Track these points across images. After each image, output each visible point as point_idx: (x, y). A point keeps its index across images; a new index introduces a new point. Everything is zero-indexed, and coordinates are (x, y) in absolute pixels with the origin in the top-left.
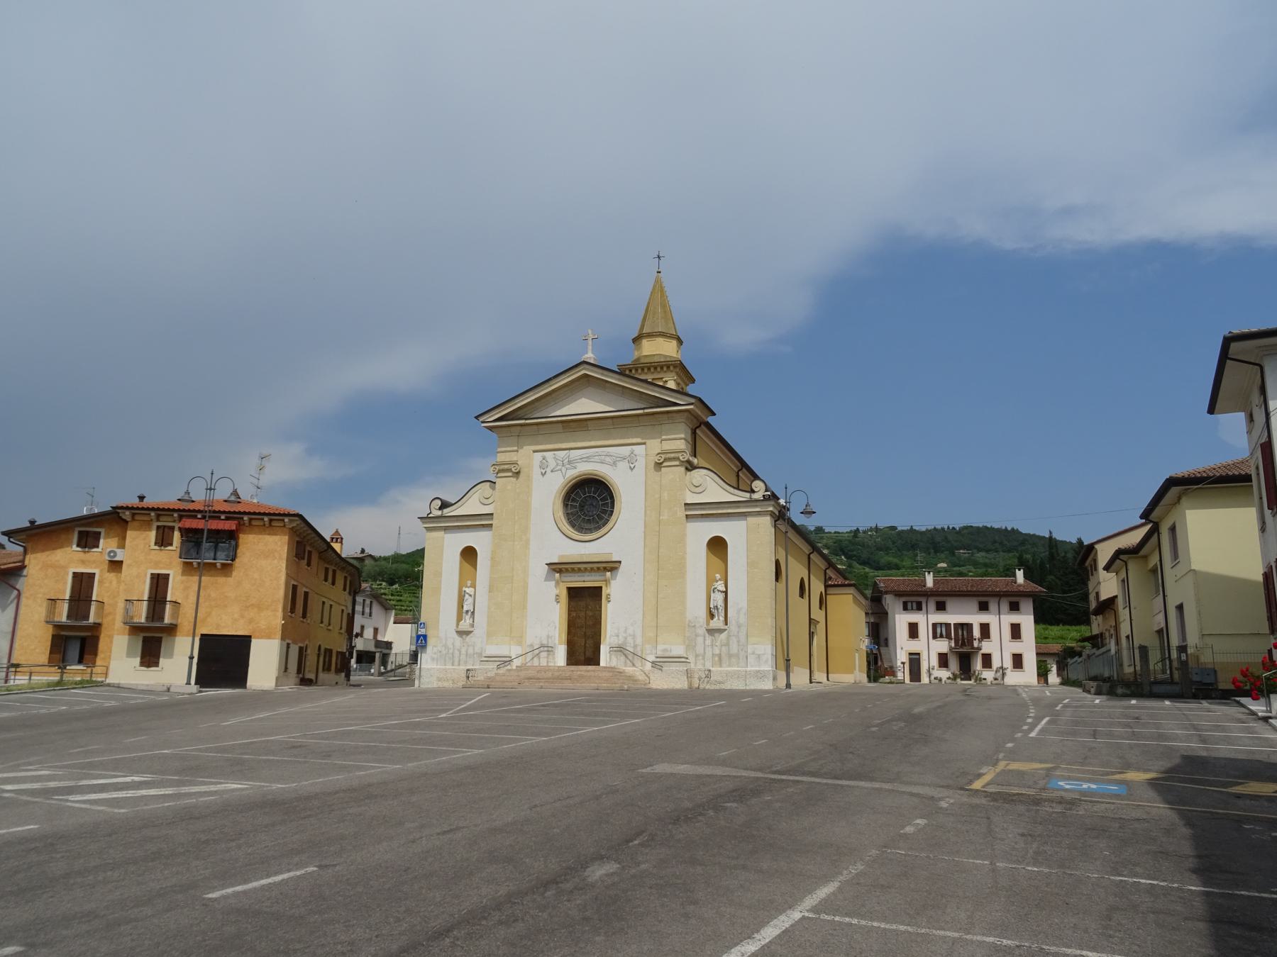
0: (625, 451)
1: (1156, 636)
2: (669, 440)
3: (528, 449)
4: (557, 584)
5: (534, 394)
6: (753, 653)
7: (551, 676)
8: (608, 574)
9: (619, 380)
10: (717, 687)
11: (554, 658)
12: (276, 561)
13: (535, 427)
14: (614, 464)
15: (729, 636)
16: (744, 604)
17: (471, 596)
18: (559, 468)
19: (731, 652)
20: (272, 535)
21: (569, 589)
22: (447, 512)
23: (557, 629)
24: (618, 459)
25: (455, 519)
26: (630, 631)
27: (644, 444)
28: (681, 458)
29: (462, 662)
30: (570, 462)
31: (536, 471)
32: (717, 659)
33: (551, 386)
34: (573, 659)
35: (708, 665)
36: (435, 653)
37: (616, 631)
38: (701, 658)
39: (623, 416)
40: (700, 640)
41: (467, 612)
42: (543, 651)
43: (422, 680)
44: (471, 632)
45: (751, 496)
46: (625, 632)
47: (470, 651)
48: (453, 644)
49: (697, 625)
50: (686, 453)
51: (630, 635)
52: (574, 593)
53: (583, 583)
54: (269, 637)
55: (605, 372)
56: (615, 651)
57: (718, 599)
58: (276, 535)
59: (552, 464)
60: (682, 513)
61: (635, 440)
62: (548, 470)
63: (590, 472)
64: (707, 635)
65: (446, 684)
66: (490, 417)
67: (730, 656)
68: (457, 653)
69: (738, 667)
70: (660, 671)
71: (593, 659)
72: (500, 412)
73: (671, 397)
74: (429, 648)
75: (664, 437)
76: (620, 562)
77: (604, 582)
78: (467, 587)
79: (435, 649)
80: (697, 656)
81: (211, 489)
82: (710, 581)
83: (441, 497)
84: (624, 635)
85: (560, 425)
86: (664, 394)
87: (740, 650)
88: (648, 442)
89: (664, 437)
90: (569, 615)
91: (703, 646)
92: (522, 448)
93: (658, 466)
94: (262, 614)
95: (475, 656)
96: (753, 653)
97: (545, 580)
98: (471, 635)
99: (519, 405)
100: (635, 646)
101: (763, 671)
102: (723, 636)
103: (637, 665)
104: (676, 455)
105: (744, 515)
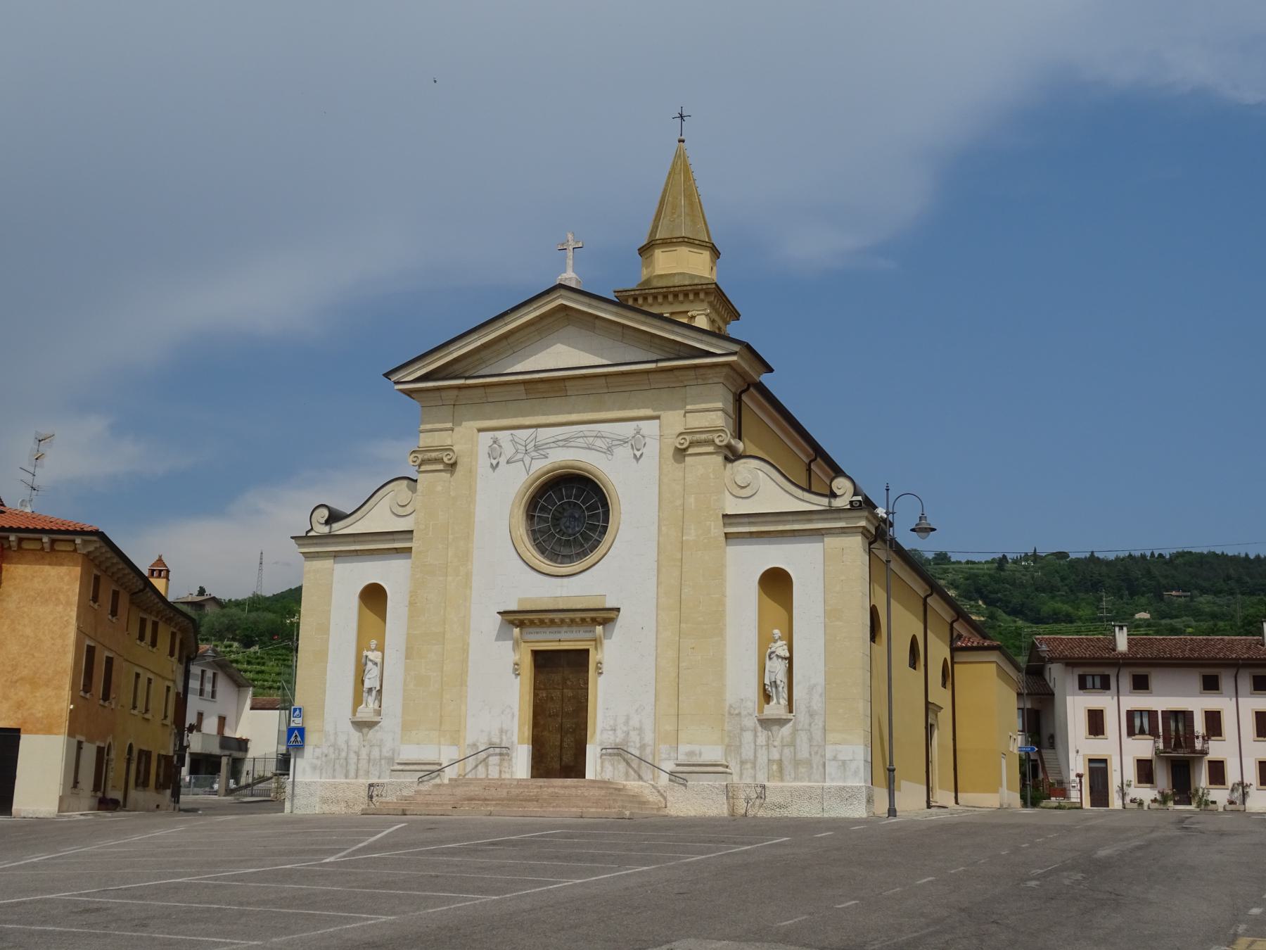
0: (627, 429)
3: (471, 425)
4: (516, 644)
5: (479, 338)
6: (835, 759)
8: (599, 629)
9: (617, 314)
10: (777, 813)
11: (510, 766)
12: (60, 608)
13: (481, 391)
14: (609, 450)
15: (795, 731)
16: (819, 679)
17: (376, 664)
18: (519, 456)
22: (338, 527)
25: (370, 538)
26: (635, 722)
27: (658, 417)
29: (361, 773)
30: (536, 448)
31: (483, 462)
32: (775, 767)
35: (762, 778)
36: (318, 758)
37: (612, 723)
38: (749, 766)
40: (748, 736)
41: (370, 690)
42: (492, 755)
43: (295, 801)
45: (830, 502)
46: (627, 723)
47: (376, 753)
48: (347, 742)
49: (744, 713)
52: (544, 661)
53: (557, 643)
54: (48, 730)
55: (595, 303)
57: (777, 669)
58: (61, 564)
59: (508, 450)
60: (718, 529)
62: (503, 460)
64: (759, 728)
67: (797, 763)
68: (353, 757)
69: (810, 781)
70: (684, 788)
71: (575, 768)
72: (424, 366)
74: (309, 750)
75: (689, 407)
76: (618, 610)
78: (369, 649)
79: (318, 752)
80: (743, 763)
82: (765, 640)
84: (625, 729)
85: (522, 388)
87: (813, 753)
89: (689, 407)
90: (535, 695)
91: (753, 746)
93: (681, 453)
94: (38, 694)
95: (383, 762)
96: (835, 759)
98: (376, 728)
99: (455, 355)
100: (643, 747)
101: (851, 788)
102: (786, 730)
103: (645, 778)
105: (819, 534)
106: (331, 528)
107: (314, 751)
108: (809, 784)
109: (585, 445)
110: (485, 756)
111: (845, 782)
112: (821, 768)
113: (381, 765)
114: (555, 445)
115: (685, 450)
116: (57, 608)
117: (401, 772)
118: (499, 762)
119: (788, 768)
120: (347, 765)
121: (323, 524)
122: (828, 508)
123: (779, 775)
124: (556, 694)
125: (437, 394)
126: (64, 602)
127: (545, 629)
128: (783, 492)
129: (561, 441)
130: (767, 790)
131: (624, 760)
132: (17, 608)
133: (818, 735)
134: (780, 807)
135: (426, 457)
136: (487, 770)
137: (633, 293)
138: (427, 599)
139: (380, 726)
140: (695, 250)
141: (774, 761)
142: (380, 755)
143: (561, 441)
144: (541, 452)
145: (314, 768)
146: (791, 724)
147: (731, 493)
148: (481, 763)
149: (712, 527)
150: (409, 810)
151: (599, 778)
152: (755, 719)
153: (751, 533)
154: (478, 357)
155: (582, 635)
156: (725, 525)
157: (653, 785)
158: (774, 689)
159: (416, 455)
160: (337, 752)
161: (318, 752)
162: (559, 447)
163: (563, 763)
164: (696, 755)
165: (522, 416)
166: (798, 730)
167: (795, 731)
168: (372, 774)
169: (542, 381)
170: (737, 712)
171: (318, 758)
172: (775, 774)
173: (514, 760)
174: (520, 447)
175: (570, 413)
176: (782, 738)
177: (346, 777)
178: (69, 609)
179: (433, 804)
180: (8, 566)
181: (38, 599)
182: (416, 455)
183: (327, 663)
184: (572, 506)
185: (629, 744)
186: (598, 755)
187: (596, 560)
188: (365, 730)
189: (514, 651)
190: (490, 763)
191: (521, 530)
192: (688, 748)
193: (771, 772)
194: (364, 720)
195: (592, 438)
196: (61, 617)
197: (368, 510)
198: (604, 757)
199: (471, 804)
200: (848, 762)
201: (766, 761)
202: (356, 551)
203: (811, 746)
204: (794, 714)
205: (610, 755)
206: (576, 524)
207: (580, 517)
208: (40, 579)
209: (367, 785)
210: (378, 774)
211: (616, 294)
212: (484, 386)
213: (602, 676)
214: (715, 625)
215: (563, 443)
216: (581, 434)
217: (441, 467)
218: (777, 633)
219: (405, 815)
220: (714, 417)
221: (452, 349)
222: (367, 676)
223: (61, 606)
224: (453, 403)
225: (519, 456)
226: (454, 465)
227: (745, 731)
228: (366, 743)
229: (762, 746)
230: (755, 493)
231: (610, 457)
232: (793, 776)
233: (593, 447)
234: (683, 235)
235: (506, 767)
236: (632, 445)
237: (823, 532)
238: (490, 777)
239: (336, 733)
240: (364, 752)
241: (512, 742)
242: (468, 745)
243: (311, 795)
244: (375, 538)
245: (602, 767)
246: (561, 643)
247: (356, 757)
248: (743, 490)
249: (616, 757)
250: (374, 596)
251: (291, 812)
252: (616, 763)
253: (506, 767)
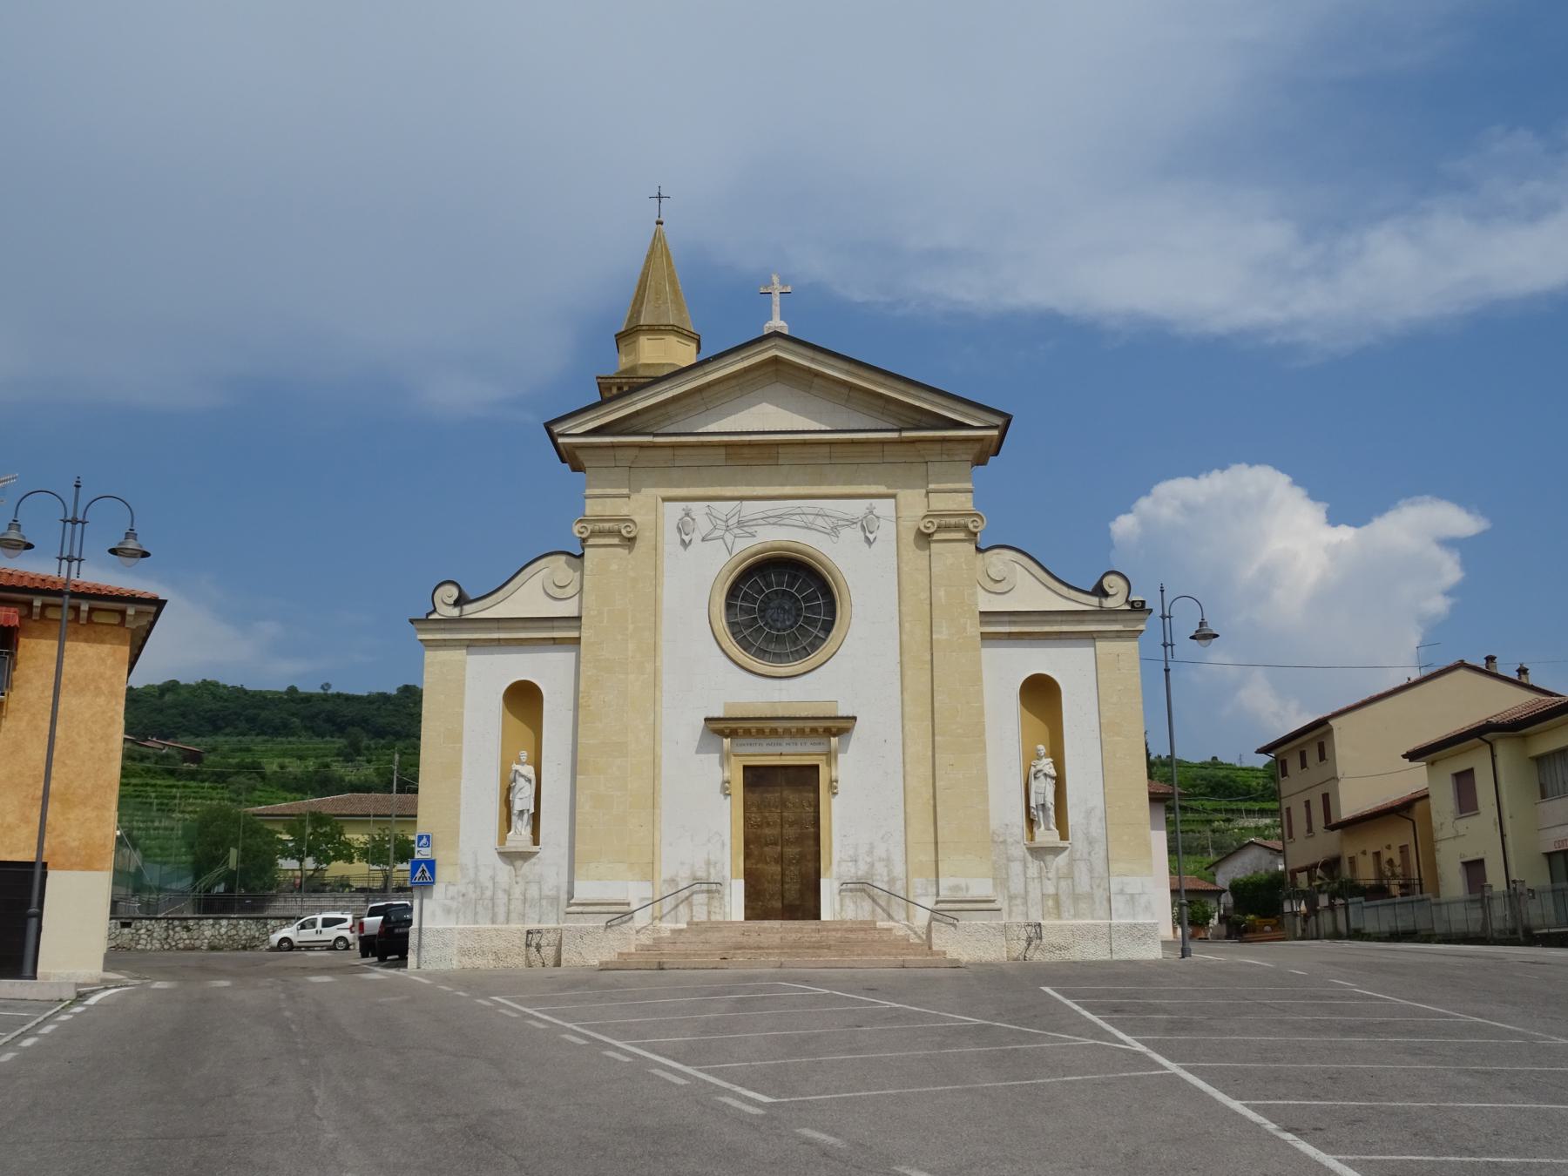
0: (857, 508)
1: (1545, 862)
2: (955, 491)
3: (650, 494)
4: (725, 759)
5: (671, 388)
6: (1122, 892)
7: (778, 941)
8: (834, 740)
9: (848, 373)
10: (1056, 957)
11: (722, 906)
12: (101, 700)
13: (669, 452)
14: (835, 531)
15: (1072, 861)
16: (1098, 801)
17: (529, 781)
18: (718, 533)
19: (1079, 890)
20: (95, 641)
21: (746, 768)
22: (470, 610)
23: (728, 848)
24: (840, 523)
25: (520, 624)
26: (880, 851)
27: (893, 496)
28: (971, 526)
29: (514, 916)
30: (740, 524)
31: (670, 537)
32: (1050, 903)
33: (706, 374)
34: (757, 906)
35: (1035, 917)
36: (452, 898)
37: (851, 852)
38: (1019, 901)
39: (853, 442)
40: (1016, 867)
41: (521, 812)
42: (697, 892)
43: (423, 953)
44: (534, 854)
45: (1100, 602)
46: (870, 852)
47: (533, 892)
48: (493, 878)
49: (1010, 840)
50: (983, 521)
51: (881, 860)
52: (756, 778)
53: (778, 758)
54: (87, 865)
55: (820, 357)
56: (851, 890)
57: (1044, 790)
58: (102, 642)
59: (703, 525)
60: (975, 629)
61: (873, 489)
62: (697, 537)
63: (784, 544)
64: (1029, 858)
65: (480, 962)
66: (576, 426)
67: (1076, 898)
68: (502, 898)
69: (1093, 918)
70: (953, 929)
71: (804, 905)
72: (598, 418)
73: (954, 411)
74: (438, 889)
75: (931, 486)
76: (854, 718)
77: (824, 758)
78: (519, 762)
79: (452, 890)
80: (1011, 898)
81: (74, 521)
82: (1030, 757)
83: (461, 586)
84: (869, 860)
85: (723, 451)
86: (937, 405)
87: (1094, 887)
88: (901, 493)
89: (931, 486)
90: (746, 819)
91: (1022, 879)
92: (639, 491)
93: (924, 538)
94: (71, 816)
95: (544, 903)
96: (1122, 892)
97: (697, 752)
98: (533, 860)
99: (639, 406)
100: (892, 881)
101: (1143, 925)
102: (1062, 859)
103: (897, 918)
104: (961, 521)
105: (1091, 637)
106: (461, 611)
107: (446, 890)
108: (1093, 922)
109: (802, 524)
110: (688, 894)
111: (1134, 919)
112: (1105, 903)
113: (541, 906)
114: (764, 522)
115: (929, 535)
116: (98, 700)
117: (581, 915)
118: (707, 900)
119: (1066, 902)
120: (493, 906)
121: (450, 605)
122: (1098, 609)
123: (1055, 911)
124: (774, 816)
125: (611, 452)
126: (106, 692)
127: (762, 741)
128: (1044, 588)
129: (771, 517)
130: (1043, 929)
131: (869, 896)
132: (40, 698)
133: (1099, 866)
134: (1060, 949)
135: (597, 528)
136: (692, 910)
137: (619, 380)
138: (604, 701)
139: (538, 858)
140: (683, 341)
141: (1049, 895)
142: (540, 895)
143: (771, 517)
144: (745, 529)
145: (448, 911)
146: (1066, 853)
147: (983, 588)
148: (682, 902)
149: (968, 625)
150: (667, 962)
151: (838, 918)
152: (1024, 847)
153: (1010, 634)
154: (663, 411)
155: (809, 748)
156: (982, 623)
157: (907, 926)
158: (1041, 814)
159: (583, 525)
160: (478, 890)
161: (452, 890)
162: (770, 524)
163: (786, 902)
164: (962, 889)
165: (720, 486)
166: (1075, 860)
167: (1072, 861)
168: (529, 918)
169: (750, 445)
170: (1001, 839)
171: (452, 898)
172: (1051, 910)
173: (727, 898)
174: (719, 522)
175: (782, 485)
176: (1058, 870)
177: (493, 922)
178: (114, 703)
179: (694, 955)
180: (27, 640)
181: (70, 687)
182: (583, 525)
183: (460, 778)
184: (780, 596)
185: (874, 878)
186: (836, 891)
187: (825, 659)
188: (518, 863)
189: (722, 765)
190: (695, 902)
191: (721, 624)
192: (952, 882)
193: (1045, 909)
194: (520, 850)
195: (813, 516)
196: (103, 712)
197: (513, 589)
198: (843, 894)
199: (747, 953)
200: (1137, 896)
201: (1040, 895)
202: (499, 640)
203: (1091, 878)
204: (1070, 841)
205: (851, 890)
206: (786, 617)
207: (790, 608)
208: (73, 661)
209: (525, 932)
210: (537, 918)
211: (599, 380)
212: (673, 446)
213: (837, 797)
214: (975, 739)
215: (775, 520)
216: (799, 511)
217: (616, 541)
218: (1042, 748)
219: (662, 969)
220: (964, 499)
221: (636, 399)
222: (519, 796)
223: (103, 698)
224: (629, 465)
225: (718, 533)
226: (632, 540)
227: (1012, 861)
228: (519, 879)
229: (1033, 878)
230: (1010, 591)
231: (835, 539)
232: (1072, 912)
233: (814, 526)
234: (672, 323)
235: (715, 907)
236: (863, 526)
237: (1095, 635)
238: (695, 920)
239: (476, 867)
240: (517, 891)
241: (723, 877)
242: (664, 881)
243: (446, 945)
244: (529, 624)
245: (842, 906)
246: (783, 758)
247: (506, 897)
248: (996, 584)
249: (859, 893)
250: (524, 698)
251: (418, 968)
252: (859, 900)
253: (715, 907)
